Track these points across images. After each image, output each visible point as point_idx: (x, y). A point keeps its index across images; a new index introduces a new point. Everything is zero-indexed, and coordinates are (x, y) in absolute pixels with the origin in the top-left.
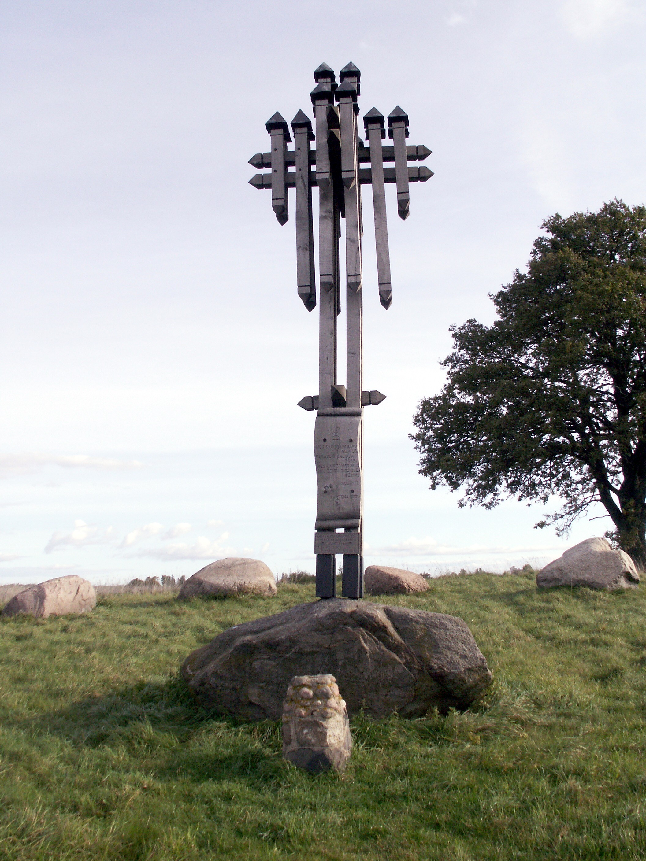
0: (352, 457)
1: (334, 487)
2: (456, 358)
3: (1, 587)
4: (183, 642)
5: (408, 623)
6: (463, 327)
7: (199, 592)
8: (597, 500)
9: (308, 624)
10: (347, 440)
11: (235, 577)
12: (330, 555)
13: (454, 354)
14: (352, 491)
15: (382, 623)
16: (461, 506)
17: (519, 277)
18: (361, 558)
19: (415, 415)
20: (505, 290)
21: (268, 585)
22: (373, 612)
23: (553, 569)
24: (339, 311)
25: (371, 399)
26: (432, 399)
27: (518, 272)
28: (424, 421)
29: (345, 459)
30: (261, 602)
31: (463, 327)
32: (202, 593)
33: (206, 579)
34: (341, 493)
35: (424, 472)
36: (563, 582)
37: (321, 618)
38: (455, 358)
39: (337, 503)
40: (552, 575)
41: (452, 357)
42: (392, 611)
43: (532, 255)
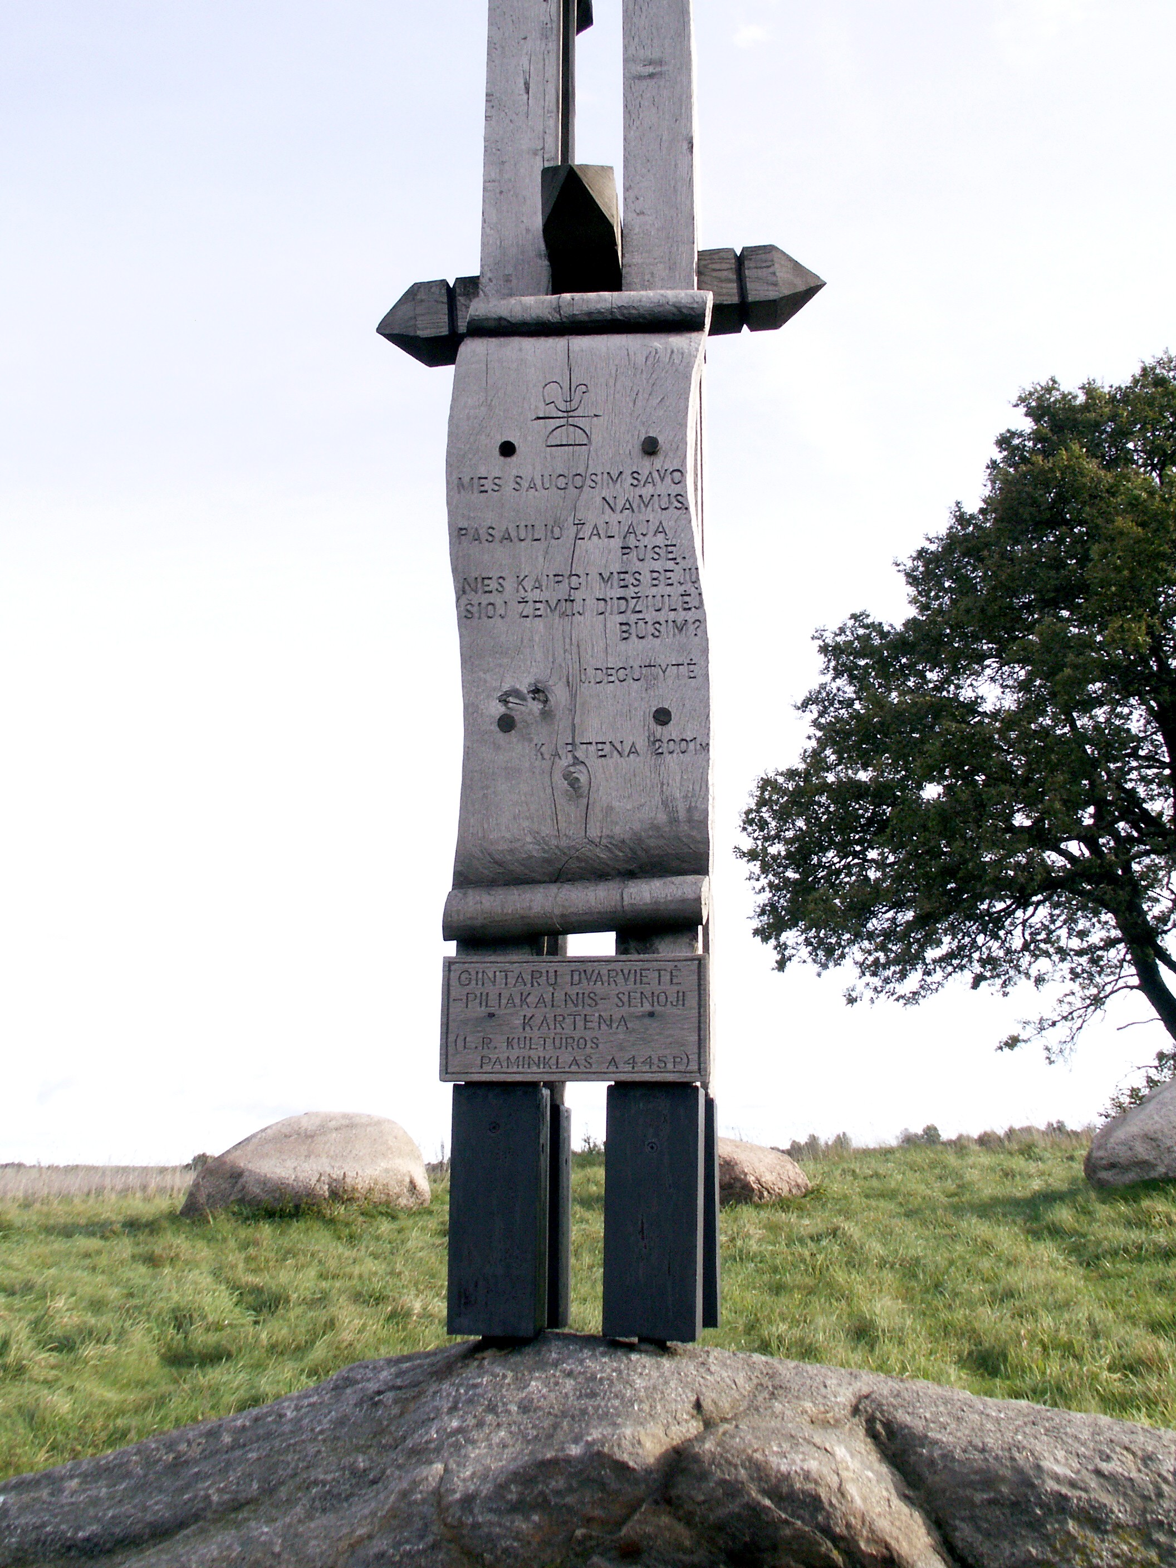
0: (660, 530)
1: (559, 695)
2: (828, 694)
3: (2, 1165)
4: (106, 1373)
5: (1035, 1526)
6: (842, 631)
7: (232, 1198)
8: (1132, 988)
9: (381, 1544)
10: (635, 445)
11: (324, 1160)
12: (534, 1085)
13: (823, 686)
14: (662, 716)
15: (876, 1539)
16: (851, 1001)
17: (962, 519)
18: (710, 1103)
19: (745, 808)
20: (933, 547)
21: (408, 1180)
22: (813, 1465)
23: (1134, 1137)
24: (586, 20)
25: (750, 286)
26: (782, 774)
27: (960, 508)
28: (763, 825)
29: (616, 543)
30: (385, 1227)
31: (840, 628)
32: (241, 1201)
33: (250, 1166)
34: (593, 729)
35: (764, 934)
36: (1162, 1169)
37: (468, 1501)
38: (824, 695)
39: (574, 783)
40: (1130, 1153)
41: (819, 692)
42: (924, 1440)
43: (989, 471)
